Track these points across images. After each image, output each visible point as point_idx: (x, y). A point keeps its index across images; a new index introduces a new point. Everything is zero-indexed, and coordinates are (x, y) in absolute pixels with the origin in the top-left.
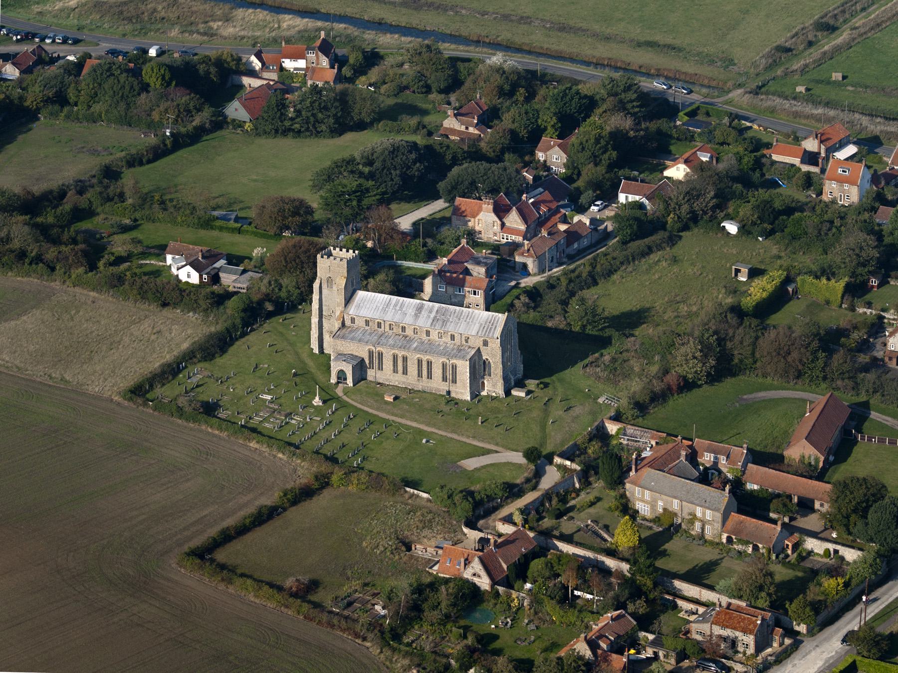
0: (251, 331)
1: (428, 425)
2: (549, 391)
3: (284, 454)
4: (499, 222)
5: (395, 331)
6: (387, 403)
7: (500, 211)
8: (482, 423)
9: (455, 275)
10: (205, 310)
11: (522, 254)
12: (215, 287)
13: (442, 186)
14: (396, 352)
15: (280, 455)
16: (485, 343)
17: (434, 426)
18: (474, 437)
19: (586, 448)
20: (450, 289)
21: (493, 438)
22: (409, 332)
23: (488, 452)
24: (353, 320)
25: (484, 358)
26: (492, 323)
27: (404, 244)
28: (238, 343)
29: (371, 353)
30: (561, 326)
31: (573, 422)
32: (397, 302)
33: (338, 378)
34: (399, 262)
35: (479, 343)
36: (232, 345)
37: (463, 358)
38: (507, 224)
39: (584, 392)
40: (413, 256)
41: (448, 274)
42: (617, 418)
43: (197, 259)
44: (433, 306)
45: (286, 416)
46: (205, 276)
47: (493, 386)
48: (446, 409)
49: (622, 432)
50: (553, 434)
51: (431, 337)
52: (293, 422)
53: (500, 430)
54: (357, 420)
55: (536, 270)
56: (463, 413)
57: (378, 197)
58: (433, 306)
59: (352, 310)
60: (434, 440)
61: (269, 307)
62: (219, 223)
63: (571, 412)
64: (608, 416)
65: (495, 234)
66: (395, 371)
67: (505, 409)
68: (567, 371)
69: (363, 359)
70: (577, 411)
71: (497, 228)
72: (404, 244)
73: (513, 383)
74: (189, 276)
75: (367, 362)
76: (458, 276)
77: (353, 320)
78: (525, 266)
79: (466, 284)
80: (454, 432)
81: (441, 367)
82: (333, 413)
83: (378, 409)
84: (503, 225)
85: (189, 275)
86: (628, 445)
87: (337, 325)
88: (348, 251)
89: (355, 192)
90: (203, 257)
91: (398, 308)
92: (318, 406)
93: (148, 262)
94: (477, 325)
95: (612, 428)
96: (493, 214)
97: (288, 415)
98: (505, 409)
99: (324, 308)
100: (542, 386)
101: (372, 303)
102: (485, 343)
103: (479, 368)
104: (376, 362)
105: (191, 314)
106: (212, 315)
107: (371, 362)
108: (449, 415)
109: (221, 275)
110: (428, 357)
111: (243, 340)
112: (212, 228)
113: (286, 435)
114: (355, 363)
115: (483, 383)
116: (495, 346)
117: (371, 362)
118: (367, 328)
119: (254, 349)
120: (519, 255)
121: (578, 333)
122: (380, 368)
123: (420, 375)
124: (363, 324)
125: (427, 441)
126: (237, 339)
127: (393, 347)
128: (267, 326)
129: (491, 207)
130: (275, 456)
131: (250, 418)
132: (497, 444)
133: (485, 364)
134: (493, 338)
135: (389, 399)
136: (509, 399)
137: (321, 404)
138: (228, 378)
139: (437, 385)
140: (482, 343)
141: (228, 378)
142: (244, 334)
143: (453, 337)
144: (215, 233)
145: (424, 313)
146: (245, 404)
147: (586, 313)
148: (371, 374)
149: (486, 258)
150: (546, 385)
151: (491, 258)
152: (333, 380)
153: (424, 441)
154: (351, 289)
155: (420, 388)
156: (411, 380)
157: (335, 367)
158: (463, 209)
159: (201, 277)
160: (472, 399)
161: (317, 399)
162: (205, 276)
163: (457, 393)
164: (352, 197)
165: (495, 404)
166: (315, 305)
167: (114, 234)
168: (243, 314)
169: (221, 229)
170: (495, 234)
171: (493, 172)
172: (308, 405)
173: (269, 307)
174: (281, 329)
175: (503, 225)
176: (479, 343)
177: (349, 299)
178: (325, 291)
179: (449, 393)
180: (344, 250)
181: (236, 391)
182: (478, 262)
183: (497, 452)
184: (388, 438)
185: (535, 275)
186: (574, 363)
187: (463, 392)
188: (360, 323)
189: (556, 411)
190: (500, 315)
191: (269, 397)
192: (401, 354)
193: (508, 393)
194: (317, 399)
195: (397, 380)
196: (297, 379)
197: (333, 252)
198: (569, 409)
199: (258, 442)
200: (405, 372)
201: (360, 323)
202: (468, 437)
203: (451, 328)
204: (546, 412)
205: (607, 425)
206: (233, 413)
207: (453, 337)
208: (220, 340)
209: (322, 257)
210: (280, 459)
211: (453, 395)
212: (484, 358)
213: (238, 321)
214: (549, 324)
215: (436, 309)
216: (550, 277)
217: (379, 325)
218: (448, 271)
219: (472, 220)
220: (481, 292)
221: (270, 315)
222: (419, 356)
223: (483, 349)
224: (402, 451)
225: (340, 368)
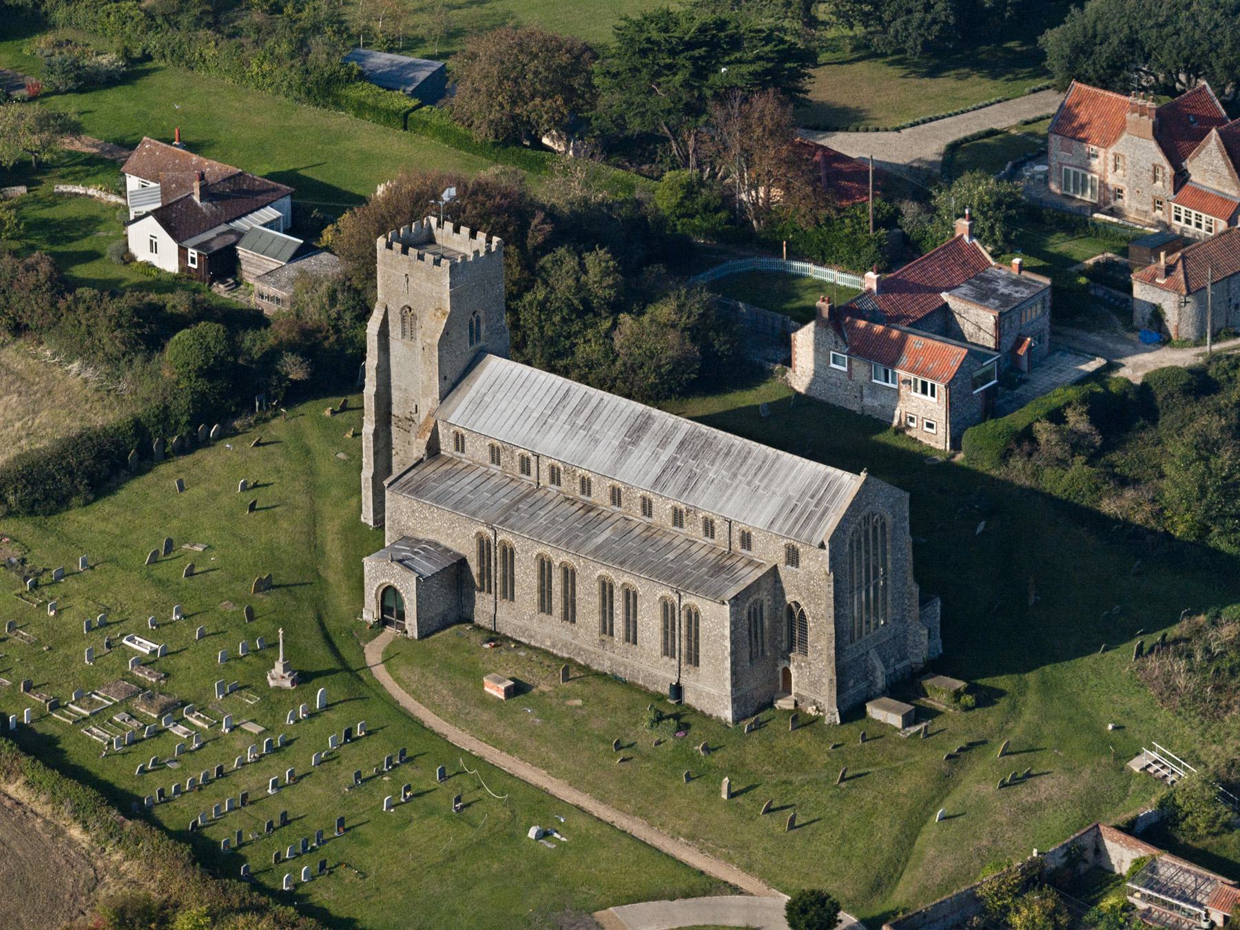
0: (221, 436)
1: (576, 783)
2: (991, 717)
3: (86, 829)
4: (1169, 170)
5: (564, 486)
6: (486, 702)
7: (1175, 136)
8: (732, 795)
9: (879, 328)
10: (111, 360)
11: (1151, 281)
12: (220, 289)
13: (1053, 40)
14: (547, 551)
15: (76, 832)
16: (793, 557)
17: (591, 788)
18: (692, 837)
19: (1006, 908)
20: (861, 369)
21: (743, 847)
22: (599, 495)
23: (710, 887)
24: (459, 442)
25: (789, 599)
26: (826, 492)
27: (823, 213)
28: (164, 469)
29: (484, 547)
30: (1138, 519)
31: (1014, 823)
32: (585, 401)
33: (385, 609)
34: (798, 265)
35: (775, 556)
36: (140, 471)
37: (715, 595)
38: (1195, 178)
39: (1099, 732)
40: (844, 251)
41: (862, 324)
42: (1159, 831)
43: (188, 200)
44: (675, 428)
45: (163, 711)
46: (192, 253)
47: (812, 679)
48: (645, 735)
49: (1145, 872)
50: (931, 852)
51: (654, 519)
52: (180, 731)
53: (777, 824)
54: (374, 744)
55: (1188, 331)
56: (692, 758)
57: (757, 67)
58: (675, 428)
59: (459, 412)
60: (567, 830)
61: (295, 369)
62: (362, 92)
63: (1023, 794)
64: (1125, 817)
65: (1158, 203)
66: (545, 605)
67: (824, 759)
68: (1088, 660)
69: (462, 563)
70: (1046, 787)
71: (1163, 187)
72: (823, 213)
73: (881, 682)
74: (153, 247)
75: (475, 569)
76: (886, 333)
77: (459, 442)
78: (1157, 314)
79: (905, 360)
80: (641, 813)
81: (658, 613)
82: (312, 715)
83: (454, 719)
84: (1181, 179)
85: (154, 248)
86: (1147, 914)
87: (418, 449)
88: (473, 235)
89: (690, 46)
90: (206, 193)
91: (580, 422)
92: (279, 689)
93: (80, 189)
94: (777, 501)
95: (1122, 854)
96: (1153, 145)
97: (173, 710)
98: (824, 759)
99: (396, 395)
100: (968, 699)
101: (516, 401)
102: (793, 557)
103: (766, 629)
104: (497, 572)
105: (75, 366)
106: (129, 375)
107: (485, 573)
108: (648, 758)
109: (242, 252)
110: (626, 579)
111: (184, 461)
112: (337, 105)
113: (122, 775)
114: (429, 568)
115: (787, 673)
116: (817, 564)
117: (485, 573)
118: (494, 469)
119: (196, 492)
120: (1143, 280)
121: (1182, 544)
122: (508, 592)
123: (607, 628)
124: (484, 455)
125: (544, 834)
126: (166, 457)
127: (538, 536)
128: (278, 427)
129: (1148, 122)
130: (59, 832)
131: (56, 706)
132: (748, 868)
133: (794, 621)
134: (809, 542)
135: (495, 690)
136: (854, 728)
137: (287, 684)
138: (62, 575)
139: (651, 666)
140: (782, 555)
141: (62, 575)
142: (192, 444)
143: (709, 528)
144: (341, 120)
145: (647, 444)
146: (67, 662)
147: (1203, 490)
148: (484, 606)
149: (1016, 283)
150: (986, 698)
151: (1028, 284)
152: (370, 614)
153: (532, 833)
154: (468, 350)
155: (605, 666)
156: (580, 639)
157: (377, 572)
158: (1083, 117)
159: (183, 253)
160: (736, 721)
161: (279, 667)
162: (192, 253)
163: (699, 695)
164: (680, 60)
165: (804, 741)
166: (370, 388)
167: (57, 92)
168: (202, 385)
169: (360, 109)
170: (1158, 203)
171: (1193, 17)
172: (254, 683)
173: (295, 369)
174: (314, 439)
175: (1181, 179)
176: (775, 556)
177: (453, 380)
178: (397, 346)
179: (677, 690)
180: (465, 231)
181: (65, 617)
182: (983, 294)
183: (736, 890)
184: (432, 811)
185: (1183, 344)
186: (1114, 639)
187: (712, 690)
188: (477, 451)
189: (979, 783)
190: (847, 476)
191: (144, 647)
192: (559, 558)
193: (852, 711)
194: (279, 667)
195: (548, 632)
196: (266, 601)
197: (437, 232)
198: (1017, 781)
199: (29, 784)
200: (570, 614)
201: (477, 451)
202: (675, 835)
203: (704, 501)
204: (944, 782)
205: (1108, 844)
206: (15, 686)
207: (709, 528)
208: (100, 455)
209: (389, 246)
210: (71, 843)
211: (689, 698)
212: (789, 599)
213: (183, 403)
214: (1108, 507)
215: (679, 437)
216: (1215, 357)
217: (525, 467)
218: (874, 317)
219: (1101, 152)
220: (940, 387)
221: (296, 395)
222: (602, 571)
223: (785, 572)
224: (452, 857)
225: (386, 581)
